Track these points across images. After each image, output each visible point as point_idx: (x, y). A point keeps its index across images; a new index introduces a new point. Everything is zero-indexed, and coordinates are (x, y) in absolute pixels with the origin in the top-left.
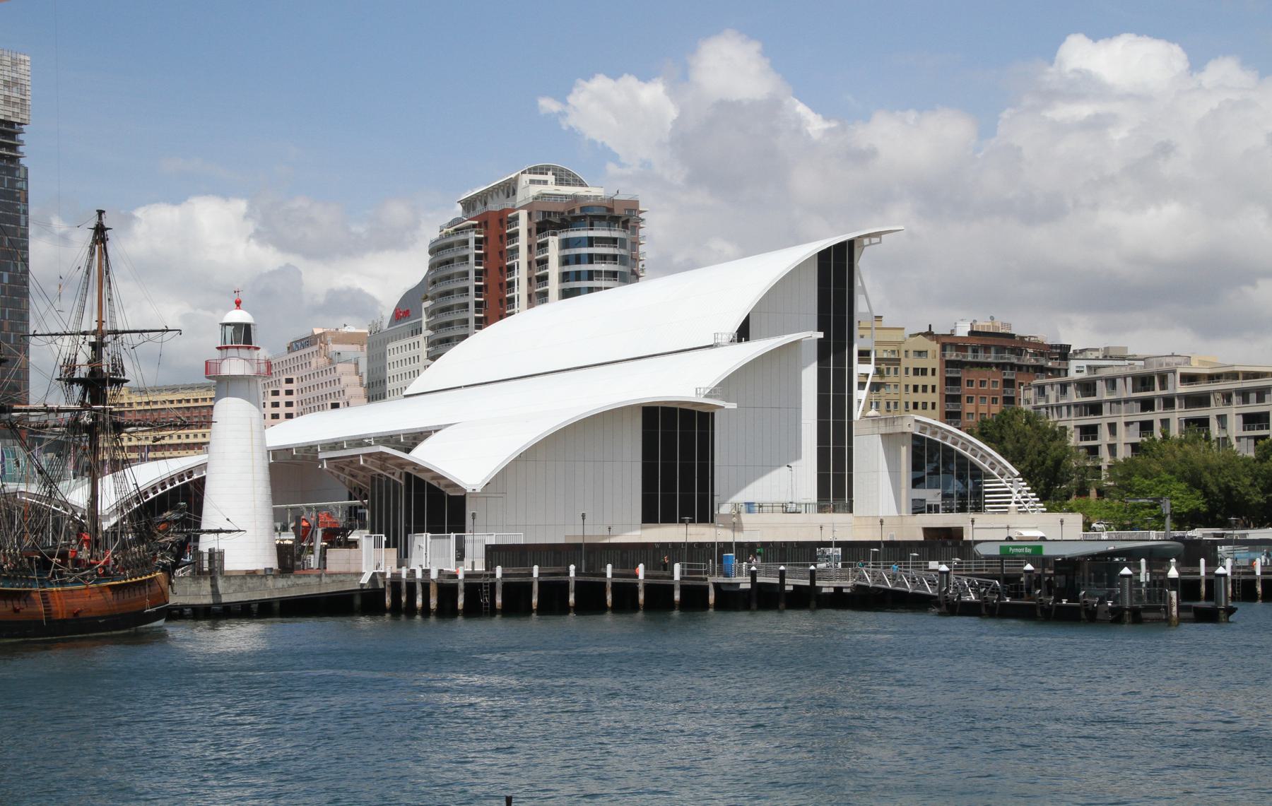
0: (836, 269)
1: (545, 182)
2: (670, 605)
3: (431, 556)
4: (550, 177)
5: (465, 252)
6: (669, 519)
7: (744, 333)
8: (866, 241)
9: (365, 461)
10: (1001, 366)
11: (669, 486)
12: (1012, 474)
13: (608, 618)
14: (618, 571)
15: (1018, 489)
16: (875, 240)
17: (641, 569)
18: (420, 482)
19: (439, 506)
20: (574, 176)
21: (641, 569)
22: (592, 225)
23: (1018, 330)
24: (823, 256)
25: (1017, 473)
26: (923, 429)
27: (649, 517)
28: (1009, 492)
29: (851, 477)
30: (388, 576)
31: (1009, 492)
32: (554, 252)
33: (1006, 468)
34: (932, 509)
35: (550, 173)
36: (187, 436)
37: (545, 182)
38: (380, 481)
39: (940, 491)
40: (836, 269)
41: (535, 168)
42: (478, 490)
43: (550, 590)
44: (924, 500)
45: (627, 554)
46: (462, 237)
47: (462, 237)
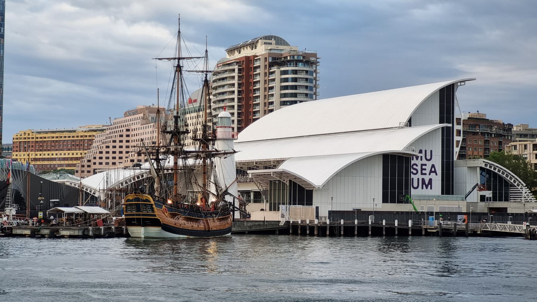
0: (447, 96)
1: (271, 44)
2: (408, 235)
3: (300, 214)
4: (273, 41)
5: (233, 74)
6: (393, 201)
7: (409, 123)
8: (459, 84)
9: (273, 175)
10: (483, 134)
11: (393, 188)
12: (522, 185)
13: (369, 239)
14: (360, 221)
15: (525, 191)
16: (462, 83)
17: (396, 222)
18: (295, 184)
19: (301, 193)
20: (284, 40)
21: (396, 222)
22: (296, 64)
23: (489, 117)
24: (442, 91)
25: (525, 185)
26: (486, 165)
27: (385, 200)
28: (522, 193)
29: (453, 185)
30: (291, 222)
31: (522, 193)
32: (277, 76)
33: (520, 182)
34: (489, 199)
35: (273, 39)
36: (49, 155)
37: (271, 44)
38: (275, 183)
39: (491, 192)
40: (447, 96)
41: (266, 37)
42: (317, 187)
43: (346, 227)
44: (485, 196)
45: (379, 214)
46: (231, 67)
47: (231, 67)
